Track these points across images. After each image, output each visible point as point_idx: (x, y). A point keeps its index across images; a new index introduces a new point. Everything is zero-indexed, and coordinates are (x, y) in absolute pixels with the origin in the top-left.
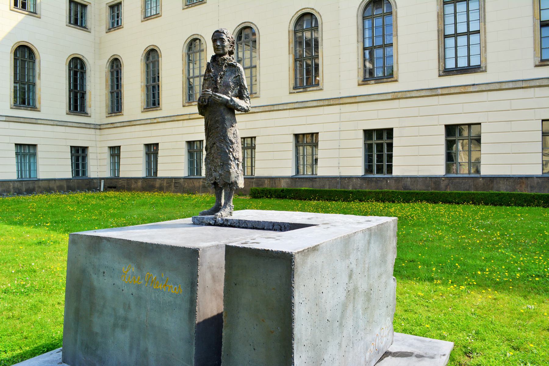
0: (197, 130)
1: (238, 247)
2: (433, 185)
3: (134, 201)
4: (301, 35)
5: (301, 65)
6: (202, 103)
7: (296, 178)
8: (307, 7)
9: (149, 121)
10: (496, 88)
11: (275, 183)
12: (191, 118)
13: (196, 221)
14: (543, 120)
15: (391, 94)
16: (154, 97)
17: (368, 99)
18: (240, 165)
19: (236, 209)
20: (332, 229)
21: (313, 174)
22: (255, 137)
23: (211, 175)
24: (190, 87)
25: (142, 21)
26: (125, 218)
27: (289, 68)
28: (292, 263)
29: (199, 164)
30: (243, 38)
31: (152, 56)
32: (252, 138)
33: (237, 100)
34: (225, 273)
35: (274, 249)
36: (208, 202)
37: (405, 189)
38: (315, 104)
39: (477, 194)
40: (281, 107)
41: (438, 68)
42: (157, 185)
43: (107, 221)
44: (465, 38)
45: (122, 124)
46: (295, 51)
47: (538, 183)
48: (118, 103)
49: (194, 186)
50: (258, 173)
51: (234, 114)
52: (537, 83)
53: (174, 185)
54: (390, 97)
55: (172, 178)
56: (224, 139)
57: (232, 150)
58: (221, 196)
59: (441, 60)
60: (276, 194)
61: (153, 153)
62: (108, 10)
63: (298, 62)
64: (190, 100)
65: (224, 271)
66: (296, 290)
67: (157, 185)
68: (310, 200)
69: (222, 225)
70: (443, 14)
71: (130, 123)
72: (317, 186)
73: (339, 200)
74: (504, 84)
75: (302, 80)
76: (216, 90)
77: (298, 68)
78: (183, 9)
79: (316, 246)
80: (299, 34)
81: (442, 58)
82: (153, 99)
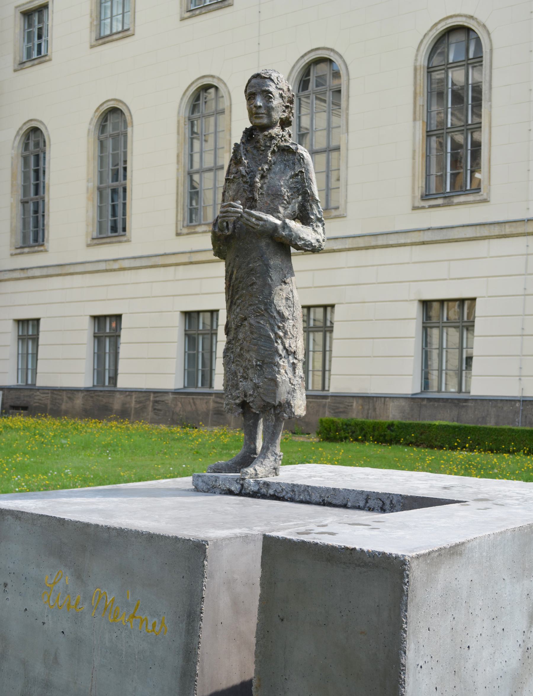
0: (208, 287)
1: (290, 541)
3: (66, 437)
4: (442, 76)
5: (440, 143)
6: (221, 230)
7: (423, 399)
8: (457, 12)
9: (102, 266)
11: (375, 410)
13: (200, 484)
16: (114, 214)
18: (300, 366)
19: (287, 462)
20: (496, 512)
21: (460, 391)
22: (333, 306)
23: (236, 386)
24: (194, 193)
25: (92, 47)
26: (46, 473)
27: (414, 151)
28: (403, 578)
29: (208, 362)
30: (312, 85)
31: (112, 120)
32: (325, 307)
33: (295, 225)
34: (261, 595)
35: (367, 548)
36: (225, 447)
38: (469, 233)
40: (392, 240)
42: (117, 406)
43: (9, 480)
45: (45, 272)
46: (429, 112)
48: (36, 225)
50: (337, 385)
51: (288, 255)
53: (151, 405)
55: (148, 392)
56: (266, 310)
57: (281, 334)
58: (256, 433)
60: (376, 433)
61: (110, 337)
62: (19, 21)
63: (434, 139)
64: (191, 221)
65: (258, 591)
66: (411, 637)
67: (117, 406)
68: (453, 448)
69: (255, 495)
71: (62, 270)
72: (469, 419)
73: (518, 451)
75: (441, 178)
76: (251, 203)
77: (434, 152)
78: (182, 19)
79: (457, 545)
80: (437, 76)
82: (112, 221)
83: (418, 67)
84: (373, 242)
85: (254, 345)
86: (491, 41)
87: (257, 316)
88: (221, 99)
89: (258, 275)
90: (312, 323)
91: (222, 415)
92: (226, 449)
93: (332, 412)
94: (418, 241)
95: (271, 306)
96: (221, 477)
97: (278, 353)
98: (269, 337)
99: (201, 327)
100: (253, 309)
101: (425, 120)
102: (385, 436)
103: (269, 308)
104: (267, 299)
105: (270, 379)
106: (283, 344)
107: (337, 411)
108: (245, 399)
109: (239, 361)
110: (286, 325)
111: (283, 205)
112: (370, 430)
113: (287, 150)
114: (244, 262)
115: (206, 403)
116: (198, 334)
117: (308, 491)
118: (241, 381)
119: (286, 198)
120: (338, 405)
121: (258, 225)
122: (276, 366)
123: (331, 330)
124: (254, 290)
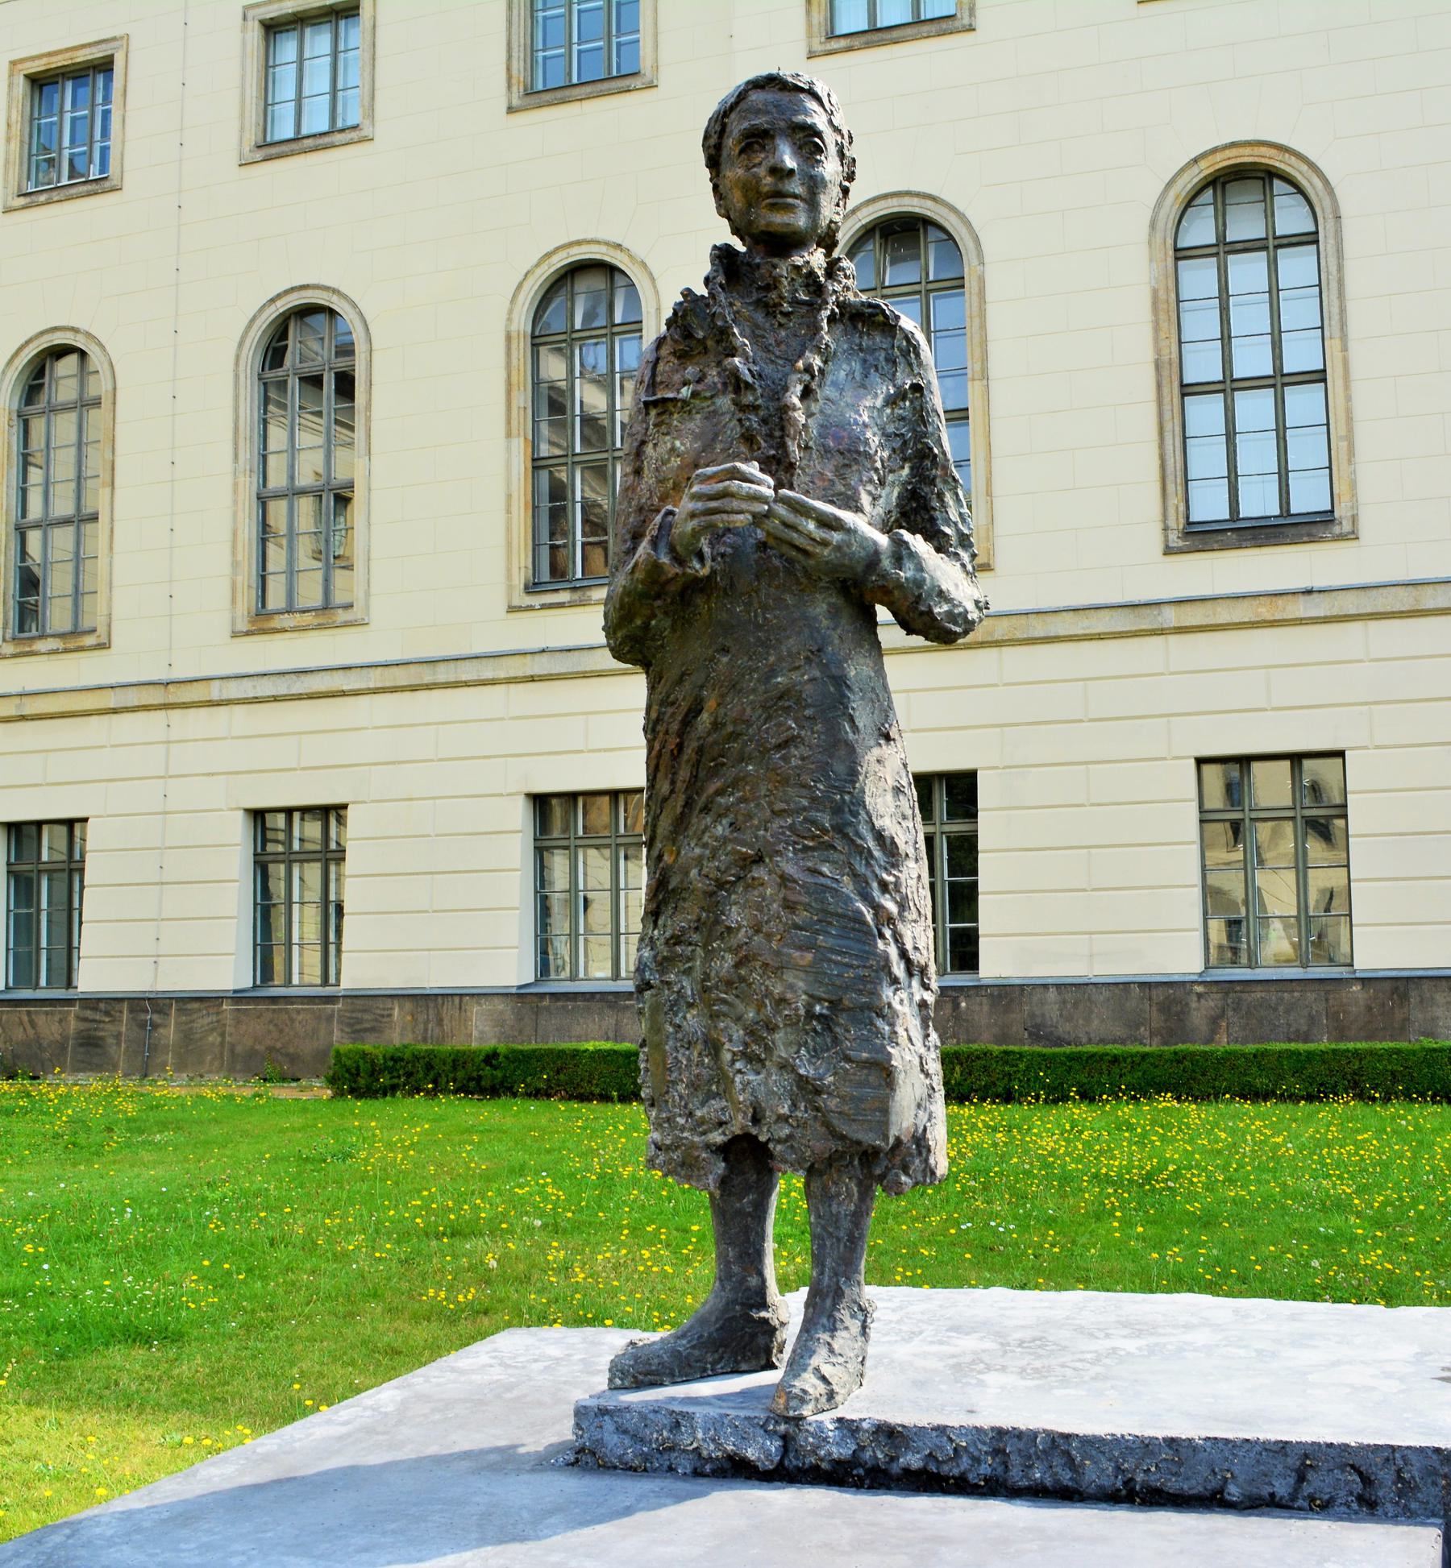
2: (1157, 1019)
7: (542, 995)
8: (589, 236)
10: (1398, 607)
11: (440, 1022)
12: (27, 711)
27: (509, 496)
37: (1036, 1036)
39: (1371, 1053)
40: (467, 672)
41: (1160, 517)
44: (1267, 397)
49: (38, 1039)
57: (892, 907)
59: (1171, 488)
60: (460, 1074)
64: (21, 630)
70: (1173, 295)
74: (1429, 590)
81: (1177, 477)
83: (514, 335)
84: (427, 675)
85: (800, 948)
86: (657, 293)
87: (806, 849)
88: (92, 378)
89: (807, 712)
90: (296, 846)
91: (97, 1046)
92: (141, 1132)
93: (347, 1030)
94: (520, 674)
95: (855, 815)
96: (699, 1412)
97: (890, 973)
98: (859, 918)
99: (45, 857)
100: (791, 828)
101: (530, 437)
102: (480, 1078)
103: (851, 824)
104: (842, 792)
105: (866, 1062)
106: (898, 938)
107: (358, 1027)
108: (754, 1131)
109: (724, 1001)
110: (902, 877)
111: (870, 487)
112: (448, 1068)
113: (872, 315)
114: (753, 670)
115: (60, 1021)
116: (39, 871)
117: (1067, 1453)
118: (739, 1071)
119: (878, 465)
120: (359, 1015)
121: (824, 543)
122: (883, 1017)
123: (340, 856)
124: (794, 762)
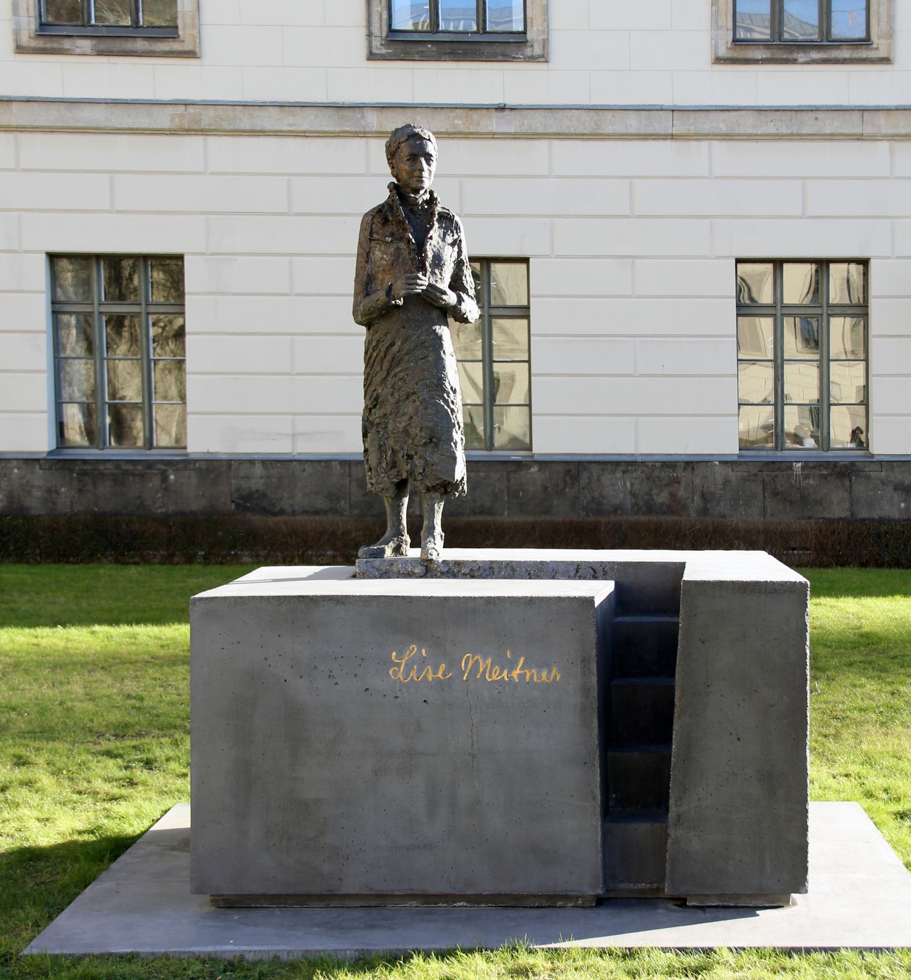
10: (580, 130)
14: (739, 261)
15: (170, 110)
17: (66, 117)
41: (364, 22)
47: (726, 482)
52: (721, 123)
54: (166, 124)
